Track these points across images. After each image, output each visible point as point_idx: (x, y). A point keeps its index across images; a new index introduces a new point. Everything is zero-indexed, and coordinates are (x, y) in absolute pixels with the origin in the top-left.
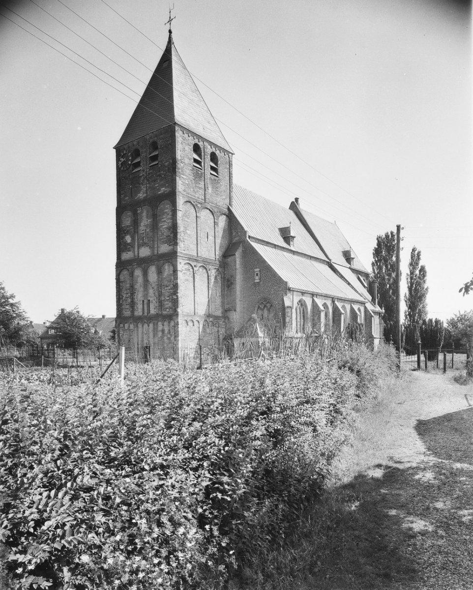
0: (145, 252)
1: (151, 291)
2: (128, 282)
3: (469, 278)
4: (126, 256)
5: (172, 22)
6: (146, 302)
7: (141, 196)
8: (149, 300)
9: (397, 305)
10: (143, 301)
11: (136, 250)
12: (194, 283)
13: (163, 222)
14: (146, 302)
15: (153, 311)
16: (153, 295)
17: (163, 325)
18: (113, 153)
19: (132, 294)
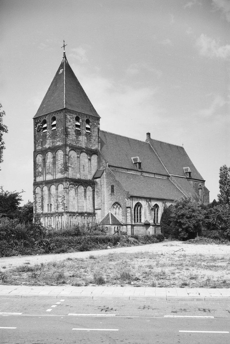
0: (49, 177)
1: (52, 199)
2: (40, 193)
3: (5, 137)
4: (39, 179)
5: (65, 47)
6: (49, 205)
7: (47, 146)
8: (51, 204)
9: (216, 238)
10: (48, 205)
11: (45, 176)
12: (119, 168)
13: (59, 161)
14: (49, 205)
15: (53, 211)
16: (53, 201)
17: (58, 218)
18: (32, 121)
19: (42, 200)
